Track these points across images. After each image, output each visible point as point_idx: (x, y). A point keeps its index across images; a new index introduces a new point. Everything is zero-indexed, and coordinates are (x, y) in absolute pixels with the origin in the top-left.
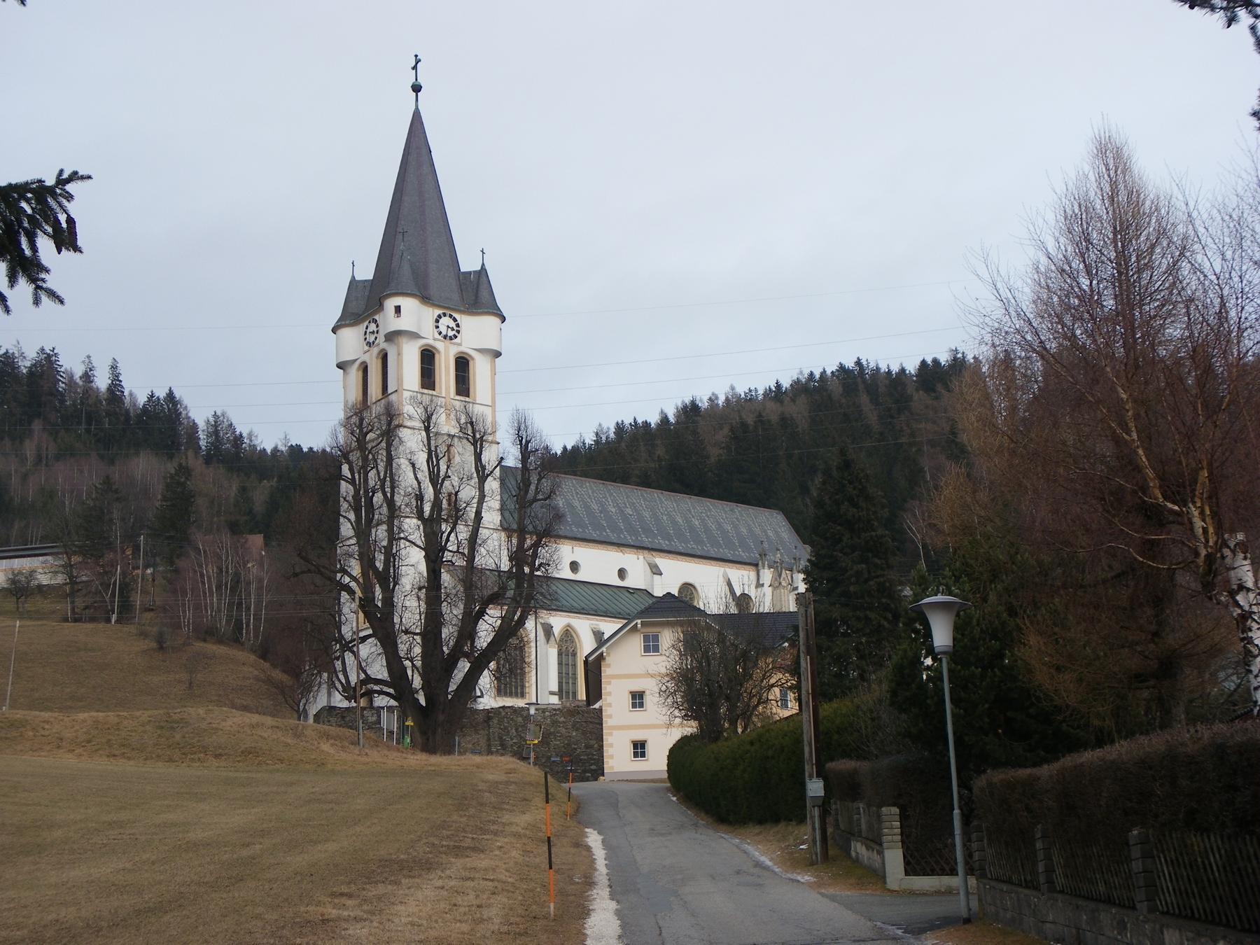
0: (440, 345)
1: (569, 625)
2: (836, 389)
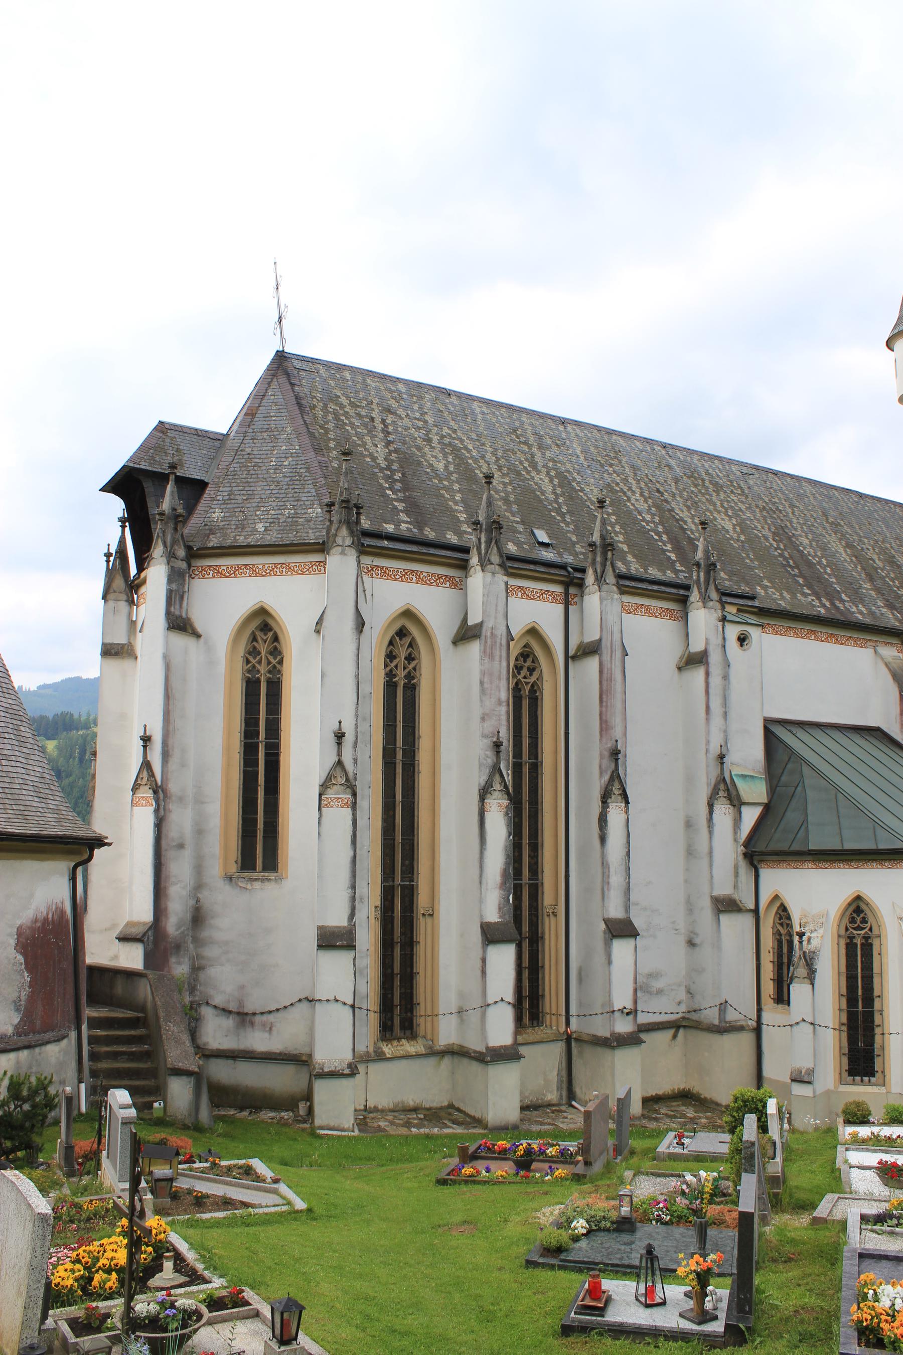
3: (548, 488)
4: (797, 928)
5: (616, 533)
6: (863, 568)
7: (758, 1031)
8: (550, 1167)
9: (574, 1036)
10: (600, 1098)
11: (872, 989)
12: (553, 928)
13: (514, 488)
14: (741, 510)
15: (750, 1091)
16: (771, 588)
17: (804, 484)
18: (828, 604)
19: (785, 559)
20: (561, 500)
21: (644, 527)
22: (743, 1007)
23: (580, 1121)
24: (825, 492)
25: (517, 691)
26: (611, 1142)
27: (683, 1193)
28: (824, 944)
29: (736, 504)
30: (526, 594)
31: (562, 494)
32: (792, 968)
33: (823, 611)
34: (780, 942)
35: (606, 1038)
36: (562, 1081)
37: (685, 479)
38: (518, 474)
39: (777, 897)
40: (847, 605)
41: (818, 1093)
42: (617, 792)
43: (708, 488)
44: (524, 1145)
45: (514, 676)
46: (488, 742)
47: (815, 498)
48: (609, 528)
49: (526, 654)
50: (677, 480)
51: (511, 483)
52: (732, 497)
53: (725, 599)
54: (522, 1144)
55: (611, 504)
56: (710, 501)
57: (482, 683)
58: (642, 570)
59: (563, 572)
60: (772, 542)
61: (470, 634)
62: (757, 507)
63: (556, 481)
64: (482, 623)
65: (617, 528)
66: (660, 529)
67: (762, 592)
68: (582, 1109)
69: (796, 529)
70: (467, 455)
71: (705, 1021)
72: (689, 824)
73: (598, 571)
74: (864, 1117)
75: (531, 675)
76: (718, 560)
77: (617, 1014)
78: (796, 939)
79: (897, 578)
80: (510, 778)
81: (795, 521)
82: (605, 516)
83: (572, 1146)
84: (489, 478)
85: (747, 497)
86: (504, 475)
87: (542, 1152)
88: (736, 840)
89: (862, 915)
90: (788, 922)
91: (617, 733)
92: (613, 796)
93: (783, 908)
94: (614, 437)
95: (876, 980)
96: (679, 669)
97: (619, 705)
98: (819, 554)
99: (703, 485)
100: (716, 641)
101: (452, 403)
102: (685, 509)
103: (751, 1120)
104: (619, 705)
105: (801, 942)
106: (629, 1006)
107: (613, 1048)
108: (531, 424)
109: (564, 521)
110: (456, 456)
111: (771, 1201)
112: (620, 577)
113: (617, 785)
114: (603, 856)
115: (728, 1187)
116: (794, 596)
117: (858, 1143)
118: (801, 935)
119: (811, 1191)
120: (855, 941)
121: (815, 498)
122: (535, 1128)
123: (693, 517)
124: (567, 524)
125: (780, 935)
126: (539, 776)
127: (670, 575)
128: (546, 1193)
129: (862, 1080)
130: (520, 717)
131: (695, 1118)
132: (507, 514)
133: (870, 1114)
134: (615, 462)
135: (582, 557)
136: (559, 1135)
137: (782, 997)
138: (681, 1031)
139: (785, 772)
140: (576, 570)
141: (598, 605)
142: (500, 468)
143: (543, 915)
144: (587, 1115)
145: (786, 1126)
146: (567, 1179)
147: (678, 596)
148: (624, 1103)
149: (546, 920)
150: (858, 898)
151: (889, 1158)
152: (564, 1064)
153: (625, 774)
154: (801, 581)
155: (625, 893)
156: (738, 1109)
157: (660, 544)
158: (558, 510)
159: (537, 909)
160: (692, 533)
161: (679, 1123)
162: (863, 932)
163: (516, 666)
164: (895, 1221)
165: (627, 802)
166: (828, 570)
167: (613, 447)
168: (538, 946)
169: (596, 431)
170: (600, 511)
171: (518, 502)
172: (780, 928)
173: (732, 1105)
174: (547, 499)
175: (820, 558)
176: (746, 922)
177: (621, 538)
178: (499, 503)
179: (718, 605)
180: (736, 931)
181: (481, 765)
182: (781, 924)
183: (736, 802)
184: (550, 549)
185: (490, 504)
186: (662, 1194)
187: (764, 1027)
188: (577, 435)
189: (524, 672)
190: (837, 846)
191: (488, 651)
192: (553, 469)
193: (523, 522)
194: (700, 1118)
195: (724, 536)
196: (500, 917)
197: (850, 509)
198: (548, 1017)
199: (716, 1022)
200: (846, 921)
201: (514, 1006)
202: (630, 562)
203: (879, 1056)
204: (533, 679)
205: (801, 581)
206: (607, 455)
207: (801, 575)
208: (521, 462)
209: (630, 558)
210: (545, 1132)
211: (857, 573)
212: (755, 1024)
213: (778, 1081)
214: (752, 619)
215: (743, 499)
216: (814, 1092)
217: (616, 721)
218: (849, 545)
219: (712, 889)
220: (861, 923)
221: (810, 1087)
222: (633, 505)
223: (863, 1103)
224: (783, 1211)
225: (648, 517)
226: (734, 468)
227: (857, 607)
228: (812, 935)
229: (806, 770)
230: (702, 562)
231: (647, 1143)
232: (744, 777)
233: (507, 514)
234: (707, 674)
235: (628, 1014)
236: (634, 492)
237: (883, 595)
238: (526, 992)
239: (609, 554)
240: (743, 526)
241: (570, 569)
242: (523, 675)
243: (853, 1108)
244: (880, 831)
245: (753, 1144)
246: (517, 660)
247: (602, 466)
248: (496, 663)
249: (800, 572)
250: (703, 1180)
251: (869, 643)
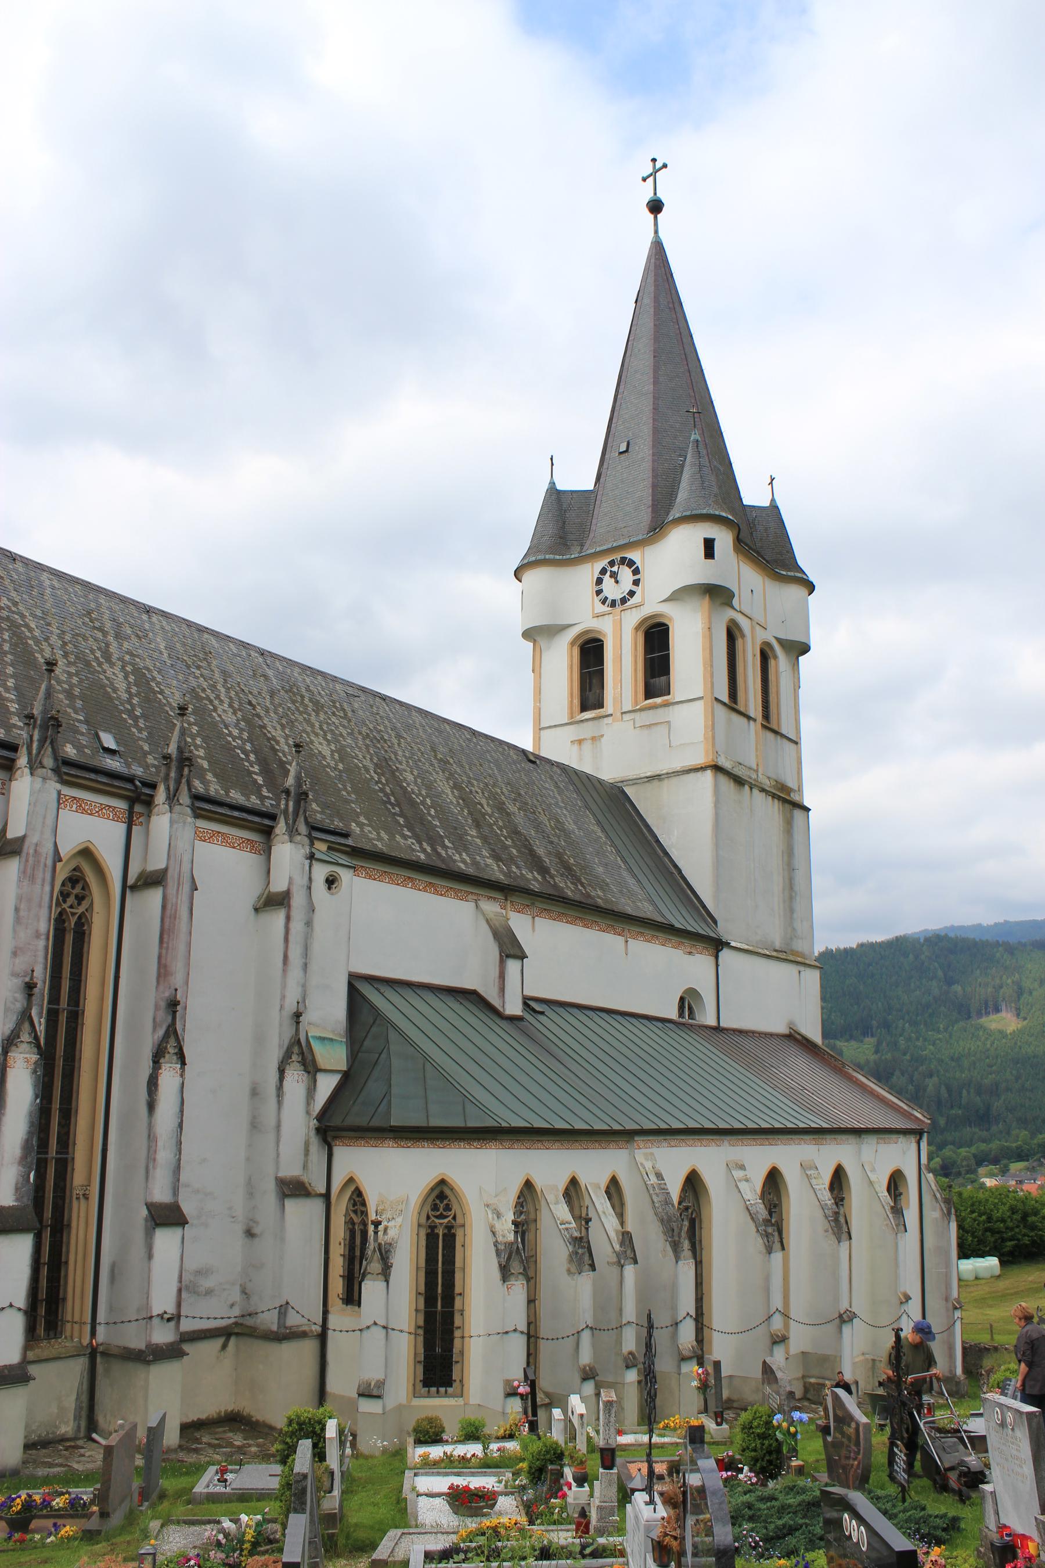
0: (605, 627)
3: (121, 686)
4: (372, 1216)
5: (197, 747)
6: (470, 813)
7: (322, 1337)
8: (55, 1525)
9: (101, 1349)
10: (127, 1428)
11: (453, 1285)
12: (82, 1214)
13: (81, 681)
14: (341, 735)
15: (309, 1411)
16: (368, 826)
17: (414, 713)
18: (429, 849)
19: (386, 795)
20: (135, 700)
21: (229, 743)
22: (306, 1311)
23: (99, 1456)
24: (436, 726)
25: (60, 921)
26: (137, 1483)
27: (219, 1544)
28: (402, 1234)
29: (337, 727)
30: (82, 808)
31: (138, 694)
32: (364, 1263)
33: (423, 857)
34: (352, 1233)
35: (140, 1351)
36: (81, 1408)
37: (282, 693)
38: (88, 664)
39: (351, 1180)
40: (450, 852)
41: (387, 1409)
42: (172, 1050)
43: (307, 706)
44: (23, 1498)
45: (58, 904)
46: (18, 982)
47: (425, 731)
48: (189, 740)
49: (75, 879)
50: (272, 694)
51: (77, 674)
52: (334, 719)
53: (315, 834)
54: (20, 1497)
55: (194, 713)
56: (308, 722)
57: (17, 910)
58: (222, 792)
59: (129, 786)
60: (373, 774)
61: (8, 849)
62: (360, 733)
63: (132, 678)
64: (24, 837)
65: (199, 741)
66: (248, 747)
67: (358, 830)
68: (103, 1442)
69: (401, 763)
70: (28, 634)
71: (262, 1327)
72: (255, 1092)
73: (172, 788)
74: (437, 1435)
75: (79, 904)
76: (311, 789)
77: (156, 1321)
78: (371, 1228)
79: (505, 827)
80: (43, 1027)
81: (400, 753)
82: (186, 725)
83: (86, 1493)
84: (51, 665)
85: (349, 721)
86: (70, 664)
87: (46, 1503)
88: (308, 1113)
89: (445, 1202)
90: (363, 1209)
91: (178, 980)
92: (167, 1056)
93: (358, 1193)
94: (206, 636)
95: (458, 1276)
96: (256, 910)
97: (182, 947)
98: (424, 792)
99: (302, 703)
100: (300, 881)
101: (15, 570)
102: (279, 727)
103: (305, 1446)
104: (182, 947)
105: (376, 1233)
106: (171, 1309)
107: (148, 1363)
108: (110, 609)
109: (136, 726)
110: (14, 634)
111: (324, 1545)
112: (196, 797)
113: (172, 1042)
114: (150, 1126)
115: (276, 1532)
116: (392, 838)
117: (430, 1466)
118: (377, 1224)
119: (372, 1528)
120: (436, 1231)
121: (425, 731)
122: (41, 1472)
123: (287, 737)
124: (140, 730)
125: (353, 1224)
126: (79, 1027)
127: (254, 801)
128: (45, 1562)
129: (438, 1392)
130: (62, 954)
131: (243, 1446)
132: (69, 710)
133: (443, 1431)
134: (204, 664)
135: (153, 770)
136: (73, 1478)
137: (352, 1297)
138: (233, 1340)
139: (370, 1036)
140: (145, 784)
141: (167, 828)
142: (66, 655)
143: (71, 1197)
144: (109, 1450)
145: (348, 1451)
146: (76, 1539)
147: (260, 826)
148: (155, 1433)
149: (75, 1203)
150: (443, 1182)
151: (460, 1481)
152: (85, 1386)
153: (184, 1030)
154: (401, 821)
155: (174, 1172)
156: (292, 1434)
157: (246, 764)
158: (131, 713)
159: (64, 1190)
160: (285, 756)
161: (225, 1453)
162: (446, 1221)
163: (61, 893)
164: (462, 1556)
165: (183, 1063)
166: (432, 812)
167: (203, 648)
168: (62, 1237)
169: (184, 626)
170: (180, 718)
171: (83, 697)
172: (353, 1215)
173: (286, 1429)
174: (119, 698)
175: (424, 798)
176: (317, 1207)
177: (201, 753)
178: (61, 696)
179: (306, 841)
180: (303, 1218)
181: (7, 1010)
182: (355, 1212)
183: (311, 1068)
184: (117, 758)
185: (48, 695)
186: (195, 1547)
187: (330, 1333)
188: (162, 628)
189: (71, 900)
190: (422, 1123)
191: (29, 871)
192: (131, 664)
193: (87, 722)
194: (250, 1446)
195: (320, 762)
196: (17, 1200)
197: (461, 746)
198: (68, 1326)
199: (275, 1328)
200: (427, 1208)
201: (26, 1312)
202: (209, 782)
203: (457, 1362)
204: (80, 910)
205: (401, 821)
206: (195, 656)
207: (402, 814)
208: (92, 651)
209: (210, 776)
210: (55, 1476)
211: (463, 817)
212: (319, 1329)
213: (343, 1397)
214: (343, 859)
215: (345, 722)
216: (384, 1408)
217: (178, 968)
218: (456, 786)
219: (277, 1169)
220: (444, 1210)
221: (379, 1402)
222: (219, 716)
223: (437, 1418)
224: (338, 1556)
225: (236, 732)
226: (338, 687)
227: (461, 855)
228: (390, 1224)
229: (393, 1035)
230: (292, 789)
231: (182, 1482)
232: (322, 1039)
233: (69, 710)
234: (288, 918)
235: (169, 1320)
236: (221, 701)
237: (490, 844)
238: (43, 1294)
239: (186, 770)
240: (342, 753)
241: (138, 783)
242: (69, 903)
243: (425, 1425)
244: (469, 1106)
245: (305, 1476)
246: (63, 884)
247: (188, 667)
248: (38, 887)
249: (401, 810)
250: (243, 1526)
251: (470, 896)
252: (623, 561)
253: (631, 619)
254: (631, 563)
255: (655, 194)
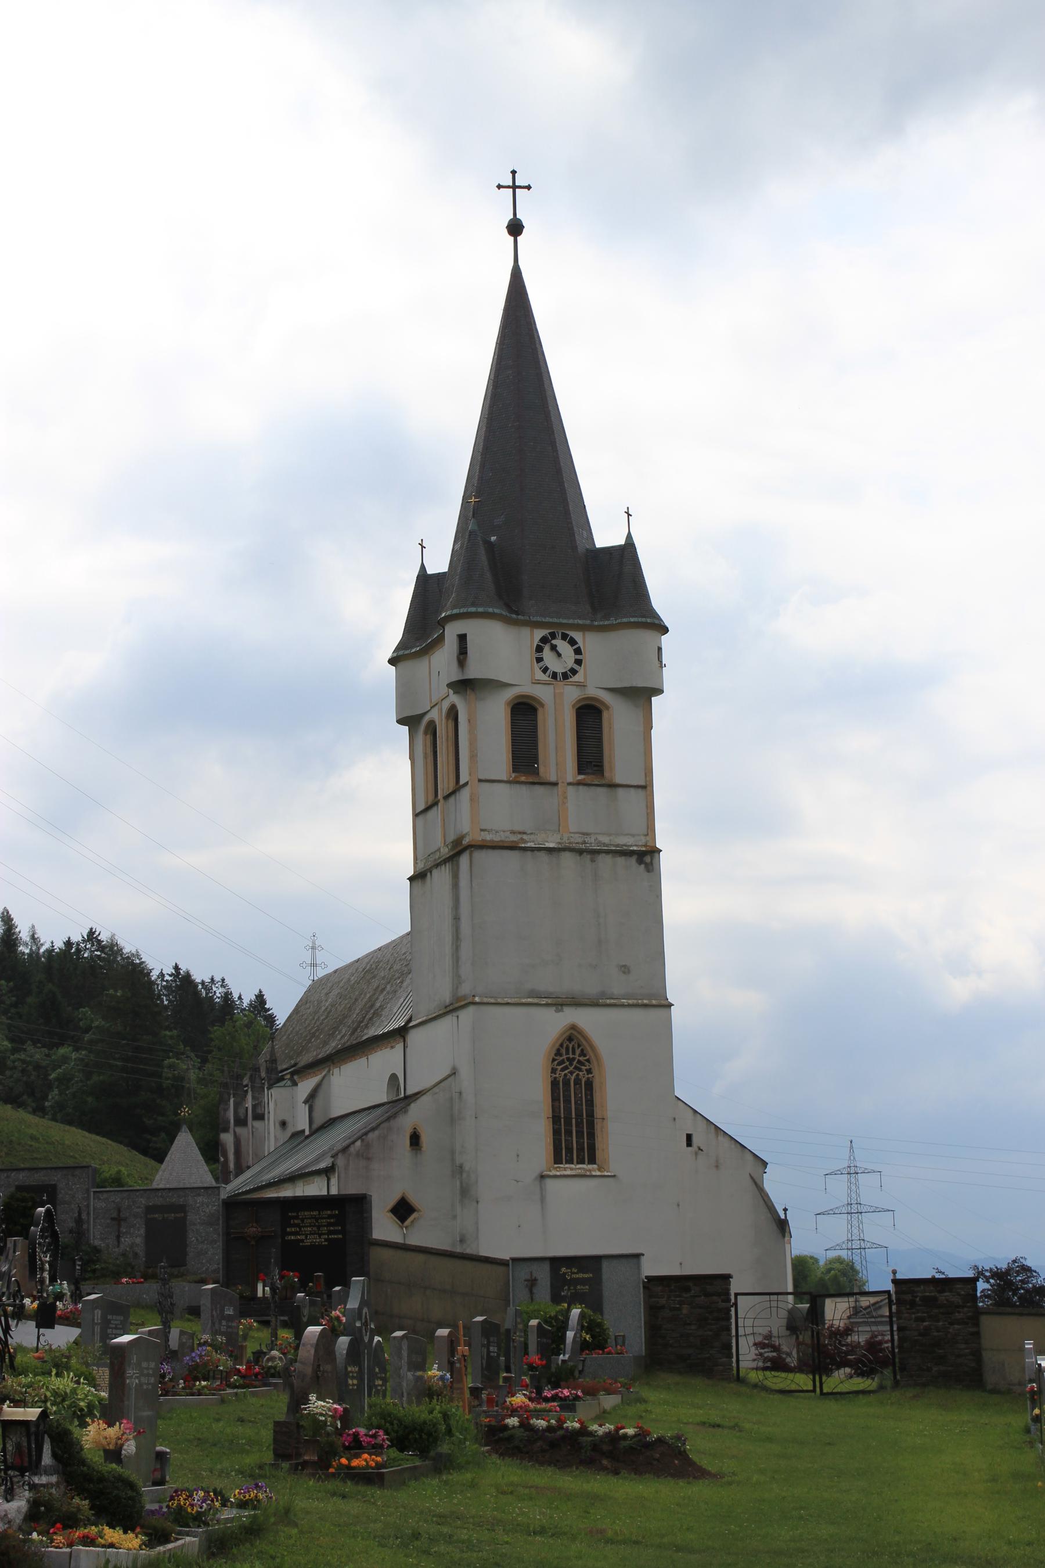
0: (543, 693)
1: (573, 1027)
2: (472, 525)
252: (564, 637)
253: (571, 695)
254: (572, 642)
255: (515, 214)
